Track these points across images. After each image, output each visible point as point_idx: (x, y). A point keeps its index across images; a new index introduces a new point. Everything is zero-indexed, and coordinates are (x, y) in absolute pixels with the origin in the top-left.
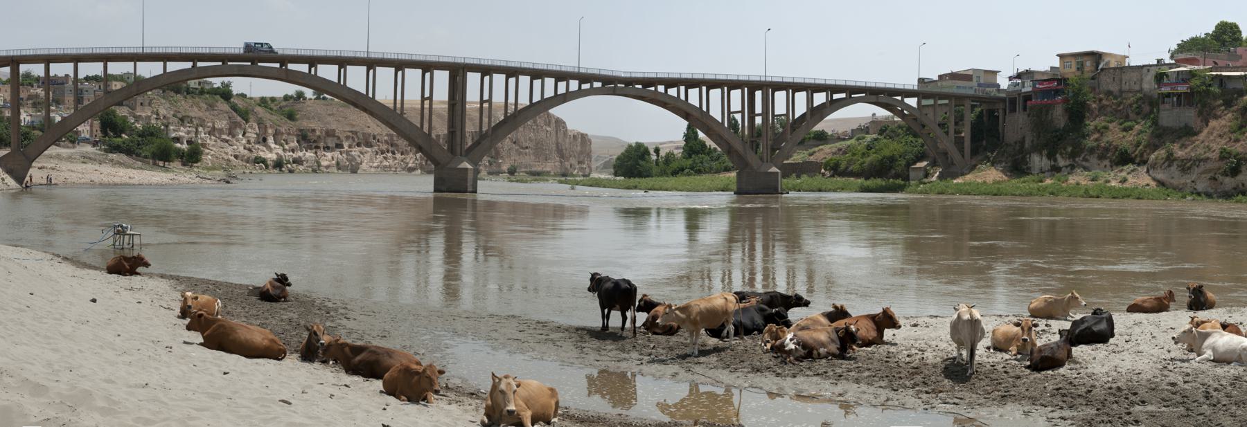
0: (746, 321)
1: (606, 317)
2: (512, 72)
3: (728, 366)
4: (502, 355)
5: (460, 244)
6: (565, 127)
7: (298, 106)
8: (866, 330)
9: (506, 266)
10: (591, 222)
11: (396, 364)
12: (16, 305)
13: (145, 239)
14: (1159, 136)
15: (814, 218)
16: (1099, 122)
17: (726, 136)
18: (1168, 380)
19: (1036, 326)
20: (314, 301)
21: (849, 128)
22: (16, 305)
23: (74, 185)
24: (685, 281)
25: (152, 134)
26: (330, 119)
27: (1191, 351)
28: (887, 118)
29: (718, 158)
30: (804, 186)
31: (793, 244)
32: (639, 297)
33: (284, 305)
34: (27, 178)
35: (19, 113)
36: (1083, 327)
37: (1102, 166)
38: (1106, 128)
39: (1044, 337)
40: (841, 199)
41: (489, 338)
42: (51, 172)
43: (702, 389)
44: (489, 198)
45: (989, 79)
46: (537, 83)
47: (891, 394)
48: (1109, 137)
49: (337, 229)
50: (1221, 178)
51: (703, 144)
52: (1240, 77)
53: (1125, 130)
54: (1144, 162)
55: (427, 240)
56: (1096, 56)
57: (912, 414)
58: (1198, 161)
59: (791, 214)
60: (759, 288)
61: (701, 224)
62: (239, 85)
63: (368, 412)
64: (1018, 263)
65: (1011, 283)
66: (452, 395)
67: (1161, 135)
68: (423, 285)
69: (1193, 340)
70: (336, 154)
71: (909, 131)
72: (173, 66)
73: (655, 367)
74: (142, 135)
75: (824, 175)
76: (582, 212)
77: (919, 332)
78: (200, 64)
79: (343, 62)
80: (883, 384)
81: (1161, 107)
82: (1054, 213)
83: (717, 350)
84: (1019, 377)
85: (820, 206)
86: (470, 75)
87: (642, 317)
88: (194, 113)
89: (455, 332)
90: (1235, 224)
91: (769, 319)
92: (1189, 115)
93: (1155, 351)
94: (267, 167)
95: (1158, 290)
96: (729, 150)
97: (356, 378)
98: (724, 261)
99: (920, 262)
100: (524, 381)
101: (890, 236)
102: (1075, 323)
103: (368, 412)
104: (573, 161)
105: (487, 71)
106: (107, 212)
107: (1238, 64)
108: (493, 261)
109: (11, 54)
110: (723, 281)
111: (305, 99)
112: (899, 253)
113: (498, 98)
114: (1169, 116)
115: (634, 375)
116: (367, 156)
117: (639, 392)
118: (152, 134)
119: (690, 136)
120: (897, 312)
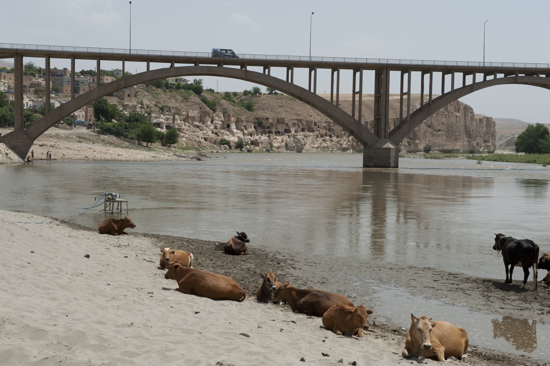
1: (509, 272)
2: (426, 69)
4: (420, 299)
5: (384, 209)
6: (472, 112)
7: (255, 99)
9: (422, 227)
10: (495, 191)
11: (333, 305)
12: (18, 262)
13: (131, 205)
20: (267, 254)
22: (18, 262)
23: (71, 160)
25: (137, 120)
26: (280, 110)
32: (540, 257)
33: (244, 257)
34: (29, 154)
35: (22, 99)
41: (408, 286)
42: (51, 149)
44: (408, 171)
46: (448, 77)
49: (286, 196)
55: (358, 206)
62: (209, 82)
63: (311, 343)
66: (378, 331)
68: (354, 242)
70: (285, 137)
72: (155, 66)
74: (129, 120)
76: (488, 183)
78: (176, 65)
79: (290, 65)
86: (392, 73)
88: (172, 103)
89: (381, 280)
94: (230, 147)
97: (301, 316)
100: (439, 322)
103: (311, 343)
104: (479, 140)
105: (406, 69)
106: (99, 183)
108: (412, 224)
109: (15, 47)
111: (260, 94)
113: (416, 90)
115: (534, 322)
116: (310, 139)
118: (137, 120)
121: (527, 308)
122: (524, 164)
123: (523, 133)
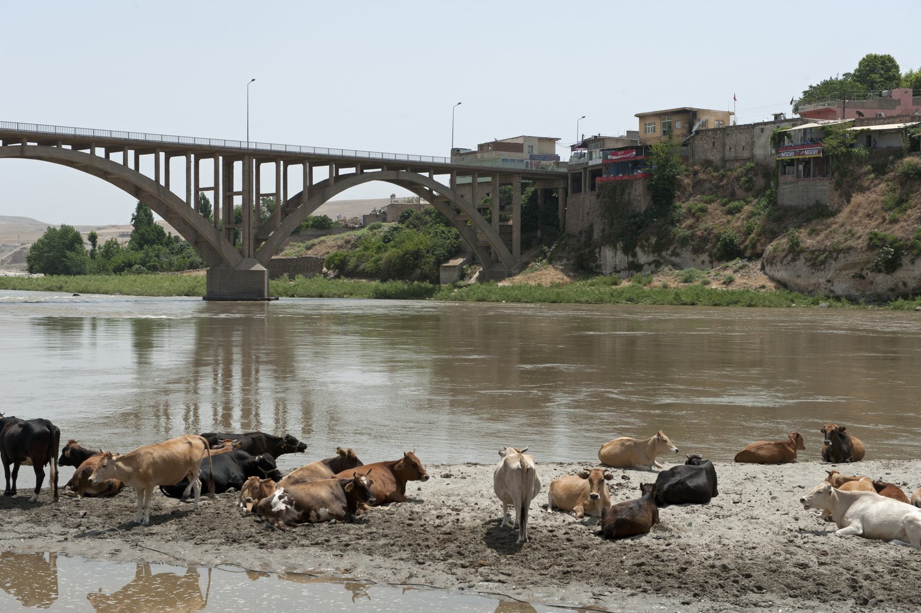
0: (218, 473)
1: (11, 476)
3: (193, 537)
8: (382, 483)
14: (779, 220)
15: (313, 333)
16: (694, 203)
17: (193, 220)
18: (795, 559)
19: (609, 478)
21: (359, 213)
24: (132, 421)
27: (830, 519)
28: (410, 200)
29: (181, 250)
30: (300, 290)
31: (284, 367)
32: (63, 444)
36: (673, 481)
37: (699, 261)
38: (704, 210)
39: (620, 493)
40: (350, 308)
43: (155, 570)
45: (545, 149)
47: (416, 569)
48: (708, 223)
50: (870, 275)
51: (160, 231)
52: (898, 130)
53: (730, 212)
54: (758, 256)
56: (689, 115)
57: (443, 595)
58: (835, 252)
59: (281, 329)
60: (237, 427)
61: (155, 340)
64: (584, 393)
65: (575, 420)
67: (781, 218)
69: (832, 505)
71: (440, 218)
73: (87, 542)
75: (326, 275)
77: (453, 485)
80: (404, 555)
81: (781, 179)
82: (632, 325)
83: (176, 515)
84: (586, 547)
85: (321, 317)
87: (67, 473)
90: (893, 340)
91: (250, 470)
92: (822, 189)
93: (776, 518)
95: (779, 432)
96: (197, 240)
98: (187, 391)
99: (454, 392)
101: (415, 356)
102: (663, 476)
107: (895, 113)
110: (186, 419)
112: (426, 380)
114: (792, 191)
115: (54, 557)
117: (62, 581)
119: (141, 219)
120: (423, 458)
121: (40, 534)
122: (43, 293)
123: (40, 241)
